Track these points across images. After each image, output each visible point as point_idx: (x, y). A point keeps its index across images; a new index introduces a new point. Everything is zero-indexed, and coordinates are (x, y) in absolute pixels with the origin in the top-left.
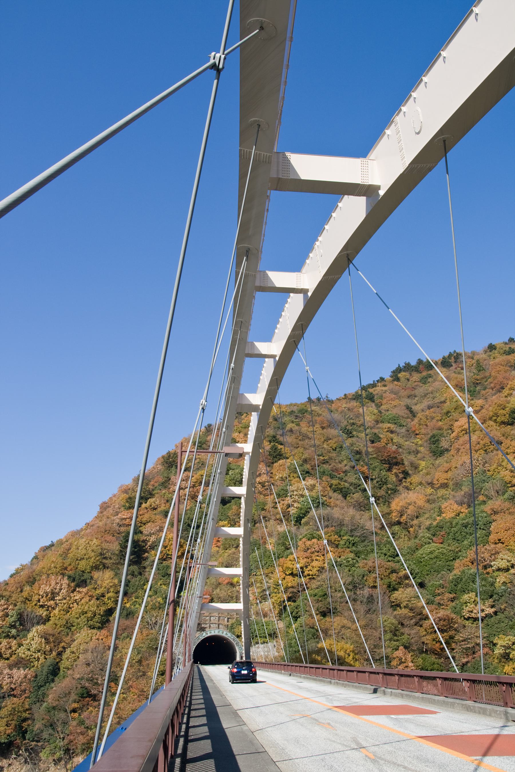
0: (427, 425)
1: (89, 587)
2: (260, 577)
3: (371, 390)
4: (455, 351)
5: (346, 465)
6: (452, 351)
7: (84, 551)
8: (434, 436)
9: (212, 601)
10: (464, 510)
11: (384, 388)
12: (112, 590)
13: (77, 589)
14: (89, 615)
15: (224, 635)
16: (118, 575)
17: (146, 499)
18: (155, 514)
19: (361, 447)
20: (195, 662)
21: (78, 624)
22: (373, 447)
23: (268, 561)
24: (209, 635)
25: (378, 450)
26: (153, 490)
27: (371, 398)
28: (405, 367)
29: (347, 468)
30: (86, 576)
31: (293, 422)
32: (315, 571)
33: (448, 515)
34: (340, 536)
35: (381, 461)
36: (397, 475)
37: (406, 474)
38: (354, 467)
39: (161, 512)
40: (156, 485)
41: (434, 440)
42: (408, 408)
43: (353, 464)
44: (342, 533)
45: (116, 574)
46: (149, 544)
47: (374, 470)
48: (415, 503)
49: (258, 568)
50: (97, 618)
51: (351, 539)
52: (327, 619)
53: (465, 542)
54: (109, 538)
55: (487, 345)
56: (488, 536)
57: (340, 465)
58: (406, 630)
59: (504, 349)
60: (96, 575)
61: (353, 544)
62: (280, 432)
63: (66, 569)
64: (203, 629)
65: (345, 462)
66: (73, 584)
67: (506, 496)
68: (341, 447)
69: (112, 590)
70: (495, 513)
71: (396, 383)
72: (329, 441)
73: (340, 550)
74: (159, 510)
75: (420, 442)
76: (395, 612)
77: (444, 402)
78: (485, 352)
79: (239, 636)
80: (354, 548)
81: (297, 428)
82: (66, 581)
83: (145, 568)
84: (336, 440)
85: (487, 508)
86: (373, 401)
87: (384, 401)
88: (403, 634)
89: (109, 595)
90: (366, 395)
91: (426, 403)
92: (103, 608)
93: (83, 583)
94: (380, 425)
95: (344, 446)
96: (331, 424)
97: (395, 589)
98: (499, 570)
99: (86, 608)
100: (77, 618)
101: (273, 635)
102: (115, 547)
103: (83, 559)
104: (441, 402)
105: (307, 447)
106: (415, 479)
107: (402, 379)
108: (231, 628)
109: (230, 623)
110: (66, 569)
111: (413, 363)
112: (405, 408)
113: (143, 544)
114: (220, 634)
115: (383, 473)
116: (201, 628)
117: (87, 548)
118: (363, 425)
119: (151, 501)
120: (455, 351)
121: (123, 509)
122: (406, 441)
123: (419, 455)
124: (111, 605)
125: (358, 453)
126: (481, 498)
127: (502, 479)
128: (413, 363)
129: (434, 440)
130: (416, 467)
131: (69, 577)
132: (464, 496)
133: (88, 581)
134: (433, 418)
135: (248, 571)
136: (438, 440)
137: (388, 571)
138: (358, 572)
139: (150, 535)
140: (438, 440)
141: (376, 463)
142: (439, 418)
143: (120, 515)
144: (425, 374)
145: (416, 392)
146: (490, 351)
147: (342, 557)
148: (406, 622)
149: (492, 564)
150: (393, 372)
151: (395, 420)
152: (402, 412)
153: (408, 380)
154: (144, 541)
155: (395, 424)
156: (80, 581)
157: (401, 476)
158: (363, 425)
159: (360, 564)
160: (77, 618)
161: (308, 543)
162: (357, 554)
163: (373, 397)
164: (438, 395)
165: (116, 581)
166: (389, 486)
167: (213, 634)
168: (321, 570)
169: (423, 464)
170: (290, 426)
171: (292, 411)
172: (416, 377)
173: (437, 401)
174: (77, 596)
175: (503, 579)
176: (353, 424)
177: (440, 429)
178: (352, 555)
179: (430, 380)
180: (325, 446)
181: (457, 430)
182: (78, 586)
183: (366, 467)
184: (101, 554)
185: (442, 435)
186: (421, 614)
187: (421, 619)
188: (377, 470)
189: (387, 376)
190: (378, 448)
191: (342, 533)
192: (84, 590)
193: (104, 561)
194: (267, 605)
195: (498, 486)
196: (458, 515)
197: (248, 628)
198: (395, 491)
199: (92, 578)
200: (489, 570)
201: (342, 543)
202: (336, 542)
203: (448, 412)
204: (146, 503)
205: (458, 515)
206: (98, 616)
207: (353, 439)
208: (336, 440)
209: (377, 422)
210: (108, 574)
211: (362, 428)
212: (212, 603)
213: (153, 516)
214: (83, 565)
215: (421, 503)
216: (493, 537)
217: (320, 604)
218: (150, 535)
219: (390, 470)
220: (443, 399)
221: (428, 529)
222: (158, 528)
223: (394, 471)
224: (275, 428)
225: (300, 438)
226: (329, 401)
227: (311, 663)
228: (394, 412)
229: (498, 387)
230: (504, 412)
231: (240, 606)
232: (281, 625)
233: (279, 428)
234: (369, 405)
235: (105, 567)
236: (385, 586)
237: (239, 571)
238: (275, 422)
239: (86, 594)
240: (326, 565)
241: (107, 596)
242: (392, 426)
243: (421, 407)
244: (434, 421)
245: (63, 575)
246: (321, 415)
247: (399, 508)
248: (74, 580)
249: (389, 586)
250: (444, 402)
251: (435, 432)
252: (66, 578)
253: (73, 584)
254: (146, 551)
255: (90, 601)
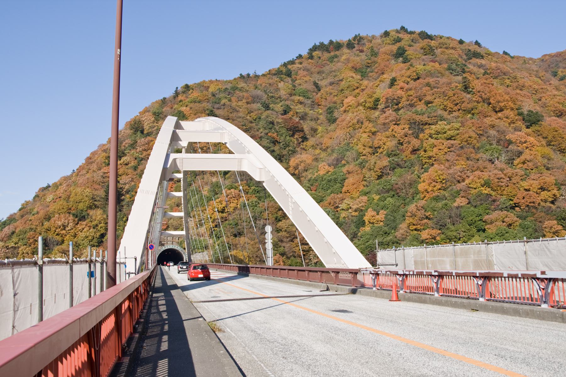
0: (326, 99)
1: (87, 221)
2: (199, 212)
3: (290, 67)
4: (359, 34)
5: (262, 132)
6: (357, 34)
7: (81, 197)
8: (330, 108)
9: (167, 229)
10: (331, 169)
11: (300, 66)
12: (102, 222)
13: (80, 223)
14: (90, 238)
15: (176, 248)
16: (105, 212)
17: (121, 157)
18: (128, 168)
19: (274, 119)
20: (158, 264)
21: (84, 244)
22: (282, 119)
23: (203, 202)
24: (167, 248)
25: (286, 121)
26: (125, 150)
27: (289, 74)
28: (319, 46)
29: (262, 134)
30: (84, 213)
31: (226, 98)
32: (231, 210)
33: (322, 173)
34: (249, 187)
35: (287, 129)
36: (297, 140)
37: (305, 139)
38: (267, 134)
39: (132, 167)
40: (127, 146)
41: (330, 111)
42: (316, 84)
43: (267, 131)
44: (251, 185)
45: (104, 211)
46: (125, 190)
47: (282, 136)
48: (305, 161)
49: (197, 206)
50: (95, 240)
51: (256, 188)
52: (237, 238)
53: (329, 191)
54: (97, 187)
55: (383, 31)
56: (342, 188)
57: (258, 133)
58: (284, 244)
59: (394, 37)
60: (91, 212)
61: (258, 192)
62: (217, 106)
63: (70, 209)
64: (163, 245)
65: (261, 130)
66: (76, 219)
67: (357, 162)
68: (260, 118)
69: (102, 222)
70: (349, 173)
71: (310, 60)
72: (252, 114)
73: (249, 195)
74: (130, 165)
75: (321, 111)
76: (279, 234)
77: (342, 80)
78: (381, 36)
79: (185, 249)
80: (258, 195)
81: (229, 103)
82: (71, 217)
83: (123, 206)
84: (256, 112)
85: (344, 170)
86: (291, 77)
87: (298, 77)
88: (280, 246)
89: (101, 225)
90: (285, 72)
91: (330, 80)
92: (98, 234)
93: (83, 218)
94: (293, 98)
95: (262, 117)
96: (255, 99)
97: (280, 220)
98: (343, 210)
99: (88, 234)
100: (83, 240)
101: (206, 247)
102: (102, 193)
103: (81, 202)
104: (340, 80)
105: (235, 118)
106: (312, 141)
107: (316, 57)
108: (181, 244)
109: (179, 241)
110: (70, 209)
111: (326, 42)
112: (312, 83)
113: (121, 190)
114: (174, 248)
115: (288, 138)
116: (161, 244)
117: (82, 193)
118: (280, 97)
119: (124, 159)
120: (359, 34)
121: (104, 165)
122: (311, 110)
123: (319, 121)
124: (103, 231)
125: (272, 123)
126: (343, 162)
127: (357, 151)
128: (326, 42)
129: (330, 111)
130: (315, 130)
131: (74, 215)
132: (333, 160)
133: (86, 217)
134: (331, 94)
135: (188, 214)
136: (332, 111)
137: (277, 210)
138: (258, 210)
139: (125, 184)
140: (332, 111)
141: (284, 131)
142: (335, 94)
143: (102, 170)
144: (332, 54)
145: (324, 69)
146: (385, 37)
147: (250, 201)
148: (285, 240)
149: (340, 205)
150: (310, 50)
151: (304, 94)
152: (311, 87)
153: (320, 58)
154: (121, 188)
155: (304, 96)
156: (81, 217)
157: (300, 140)
158: (280, 97)
159: (260, 205)
160: (83, 240)
161: (229, 191)
162: (259, 198)
163: (291, 73)
164: (338, 74)
165: (105, 216)
166: (291, 148)
167: (169, 247)
168: (235, 209)
169: (320, 129)
170: (223, 101)
171: (226, 88)
172: (326, 55)
173: (337, 79)
174: (79, 227)
175: (344, 215)
176: (272, 97)
177: (335, 103)
178: (255, 199)
179: (336, 60)
180: (248, 117)
181: (345, 105)
182: (80, 220)
183: (276, 134)
184: (93, 198)
185: (335, 108)
186: (294, 235)
187: (294, 238)
188: (284, 135)
189: (305, 53)
190: (286, 119)
191: (251, 185)
192: (84, 223)
193: (96, 203)
194: (202, 230)
195: (355, 155)
196: (328, 173)
197: (188, 244)
198: (294, 152)
199: (88, 214)
200: (338, 209)
201: (251, 191)
202: (247, 191)
203: (342, 90)
204: (120, 160)
205: (328, 173)
206: (95, 239)
207: (269, 112)
208: (256, 112)
209: (291, 95)
210: (99, 212)
211: (278, 100)
212: (168, 230)
213: (126, 170)
214: (81, 206)
215: (309, 161)
216: (344, 189)
217: (233, 230)
218: (125, 184)
219: (293, 135)
220: (341, 78)
221: (309, 181)
222: (130, 179)
223: (296, 136)
224: (213, 103)
225: (231, 111)
226: (257, 76)
227: (225, 263)
228: (304, 86)
229: (380, 72)
230: (371, 100)
231: (184, 233)
232: (211, 241)
233: (216, 102)
234: (286, 80)
235: (96, 207)
236: (274, 219)
237: (182, 214)
238: (213, 97)
239: (86, 225)
240: (238, 206)
241: (100, 226)
242: (301, 98)
243: (325, 83)
244: (332, 96)
245: (69, 213)
246: (248, 91)
247: (294, 165)
248: (77, 217)
249: (276, 219)
250: (342, 80)
251: (332, 105)
252: (71, 216)
253: (76, 219)
254: (123, 195)
255: (90, 229)
